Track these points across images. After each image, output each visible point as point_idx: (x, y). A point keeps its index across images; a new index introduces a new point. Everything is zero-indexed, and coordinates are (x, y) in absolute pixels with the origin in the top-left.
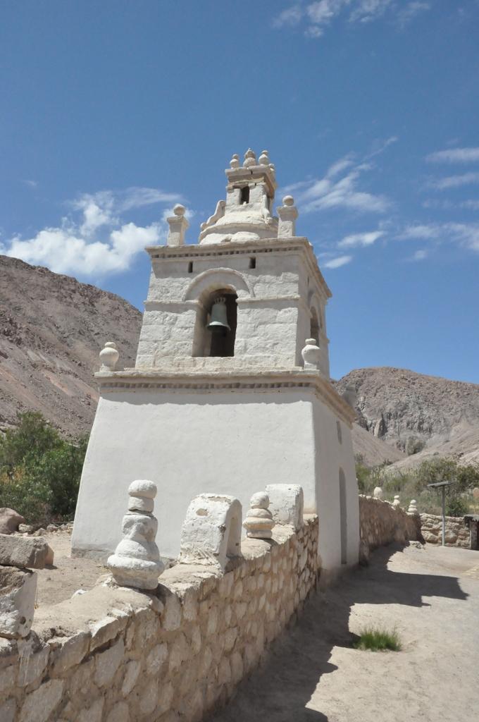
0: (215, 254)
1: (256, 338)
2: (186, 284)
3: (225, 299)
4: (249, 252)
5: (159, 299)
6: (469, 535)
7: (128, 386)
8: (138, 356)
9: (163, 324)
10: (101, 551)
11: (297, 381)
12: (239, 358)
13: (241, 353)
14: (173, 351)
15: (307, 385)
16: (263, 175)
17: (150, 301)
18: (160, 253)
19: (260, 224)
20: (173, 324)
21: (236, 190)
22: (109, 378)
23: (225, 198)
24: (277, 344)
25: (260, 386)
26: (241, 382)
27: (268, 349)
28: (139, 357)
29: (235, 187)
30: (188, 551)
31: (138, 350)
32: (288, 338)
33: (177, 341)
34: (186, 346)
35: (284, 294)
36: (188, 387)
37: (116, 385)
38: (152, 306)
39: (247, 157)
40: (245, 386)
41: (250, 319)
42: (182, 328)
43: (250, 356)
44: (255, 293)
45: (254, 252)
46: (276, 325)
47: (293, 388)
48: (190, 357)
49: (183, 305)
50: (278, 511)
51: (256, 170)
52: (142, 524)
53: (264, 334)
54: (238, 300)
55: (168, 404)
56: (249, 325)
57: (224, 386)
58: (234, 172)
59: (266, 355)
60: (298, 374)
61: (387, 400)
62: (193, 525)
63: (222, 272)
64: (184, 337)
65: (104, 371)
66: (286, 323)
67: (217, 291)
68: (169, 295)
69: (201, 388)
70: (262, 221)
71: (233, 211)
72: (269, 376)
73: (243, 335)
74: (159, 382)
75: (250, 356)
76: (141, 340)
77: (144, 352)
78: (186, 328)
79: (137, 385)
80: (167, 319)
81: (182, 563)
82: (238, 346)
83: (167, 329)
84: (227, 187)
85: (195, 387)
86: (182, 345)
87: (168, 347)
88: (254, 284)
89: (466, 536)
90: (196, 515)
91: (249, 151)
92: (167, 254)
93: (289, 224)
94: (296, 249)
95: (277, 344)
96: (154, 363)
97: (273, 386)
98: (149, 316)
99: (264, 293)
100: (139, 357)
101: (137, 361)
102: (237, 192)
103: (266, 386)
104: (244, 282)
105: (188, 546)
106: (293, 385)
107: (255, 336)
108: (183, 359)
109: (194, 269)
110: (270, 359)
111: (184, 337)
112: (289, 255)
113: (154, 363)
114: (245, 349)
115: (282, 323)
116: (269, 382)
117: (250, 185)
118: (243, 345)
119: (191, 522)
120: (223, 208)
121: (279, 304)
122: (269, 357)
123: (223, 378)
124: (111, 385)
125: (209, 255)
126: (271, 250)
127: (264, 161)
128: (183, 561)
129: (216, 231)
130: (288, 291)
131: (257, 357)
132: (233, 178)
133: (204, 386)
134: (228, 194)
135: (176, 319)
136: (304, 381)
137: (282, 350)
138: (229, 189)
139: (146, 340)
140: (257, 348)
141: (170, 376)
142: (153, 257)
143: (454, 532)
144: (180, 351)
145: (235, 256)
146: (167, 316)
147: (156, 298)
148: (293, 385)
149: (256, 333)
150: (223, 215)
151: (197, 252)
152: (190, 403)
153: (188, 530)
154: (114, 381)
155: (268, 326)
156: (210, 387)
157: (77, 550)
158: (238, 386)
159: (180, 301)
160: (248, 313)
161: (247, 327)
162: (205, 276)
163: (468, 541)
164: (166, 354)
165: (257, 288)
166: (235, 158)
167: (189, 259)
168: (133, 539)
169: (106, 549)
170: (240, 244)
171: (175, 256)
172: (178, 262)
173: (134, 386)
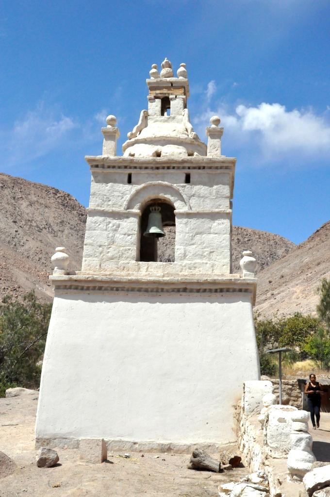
0: (152, 168)
1: (194, 246)
2: (126, 194)
3: (160, 209)
4: (184, 168)
5: (101, 207)
6: (300, 397)
7: (82, 289)
8: (84, 259)
9: (106, 230)
10: (66, 439)
11: (237, 287)
12: (180, 263)
13: (181, 260)
14: (118, 255)
15: (246, 291)
16: (183, 87)
17: (93, 208)
18: (100, 164)
19: (186, 139)
20: (116, 230)
21: (157, 100)
22: (65, 281)
23: (147, 108)
24: (213, 252)
25: (205, 291)
26: (189, 287)
27: (205, 256)
28: (86, 260)
29: (156, 97)
30: (276, 448)
31: (84, 254)
32: (222, 247)
33: (121, 246)
34: (130, 252)
35: (217, 208)
36: (139, 290)
37: (70, 287)
38: (95, 213)
39: (163, 67)
40: (191, 291)
41: (188, 229)
42: (125, 235)
43: (190, 262)
44: (191, 205)
45: (189, 168)
46: (212, 236)
47: (235, 293)
48: (134, 262)
49: (125, 213)
50: (259, 403)
51: (176, 82)
52: (308, 440)
53: (201, 243)
54: (175, 211)
55: (121, 302)
56: (187, 235)
57: (173, 290)
58: (154, 83)
59: (205, 261)
60: (239, 282)
61: (166, 245)
62: (277, 430)
63: (160, 185)
64: (127, 243)
65: (58, 275)
66: (220, 234)
67: (151, 200)
68: (110, 203)
69: (152, 291)
70: (186, 134)
71: (156, 121)
72: (214, 283)
73: (183, 243)
74: (112, 286)
75: (190, 262)
76: (86, 245)
77: (90, 256)
78: (129, 235)
79: (91, 288)
80: (111, 225)
81: (274, 458)
82: (178, 253)
83: (111, 235)
84: (148, 97)
85: (146, 291)
86: (126, 250)
87: (112, 252)
88: (190, 197)
89: (298, 397)
90: (278, 423)
91: (166, 60)
92: (106, 165)
93: (216, 142)
94: (227, 168)
95: (213, 252)
96: (100, 265)
97: (216, 291)
98: (92, 222)
99: (199, 206)
100: (86, 260)
101: (83, 264)
102: (158, 102)
103: (210, 291)
104: (182, 196)
105: (276, 445)
106: (234, 290)
107: (193, 244)
108: (128, 263)
109: (133, 180)
110: (208, 265)
111: (127, 243)
112: (220, 173)
113: (100, 265)
114: (185, 255)
115: (216, 234)
116: (213, 287)
117: (171, 97)
118: (183, 252)
119: (276, 428)
120: (146, 117)
121: (213, 216)
122: (207, 263)
123: (173, 284)
124: (65, 287)
125: (146, 168)
126: (204, 168)
127: (183, 74)
128: (274, 457)
129: (145, 141)
130: (220, 205)
131: (195, 264)
132: (153, 88)
133: (155, 290)
134: (150, 104)
135: (119, 226)
136: (243, 288)
137: (218, 257)
138: (150, 99)
139: (91, 245)
140: (195, 255)
141: (124, 280)
142: (92, 166)
143: (288, 394)
144: (124, 256)
145: (171, 171)
146: (110, 222)
147: (98, 205)
148: (234, 290)
149: (193, 242)
150: (146, 126)
151: (135, 165)
152: (141, 302)
153: (275, 434)
154: (69, 284)
155: (204, 236)
156: (160, 290)
157: (42, 439)
158: (185, 290)
159: (122, 209)
160: (186, 224)
161: (185, 236)
162: (144, 188)
163: (301, 402)
164: (112, 258)
165: (193, 201)
166: (155, 68)
167: (128, 171)
168: (304, 450)
169: (71, 437)
170: (176, 161)
171: (114, 167)
172: (117, 173)
173: (88, 288)
